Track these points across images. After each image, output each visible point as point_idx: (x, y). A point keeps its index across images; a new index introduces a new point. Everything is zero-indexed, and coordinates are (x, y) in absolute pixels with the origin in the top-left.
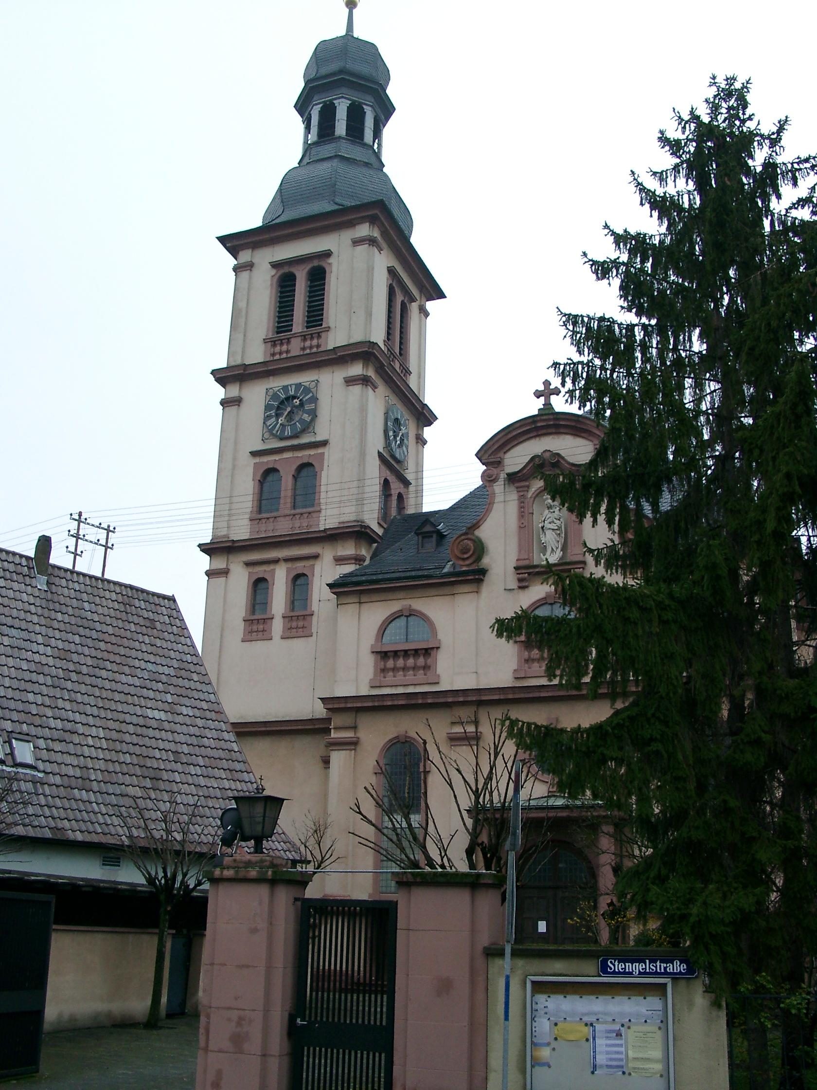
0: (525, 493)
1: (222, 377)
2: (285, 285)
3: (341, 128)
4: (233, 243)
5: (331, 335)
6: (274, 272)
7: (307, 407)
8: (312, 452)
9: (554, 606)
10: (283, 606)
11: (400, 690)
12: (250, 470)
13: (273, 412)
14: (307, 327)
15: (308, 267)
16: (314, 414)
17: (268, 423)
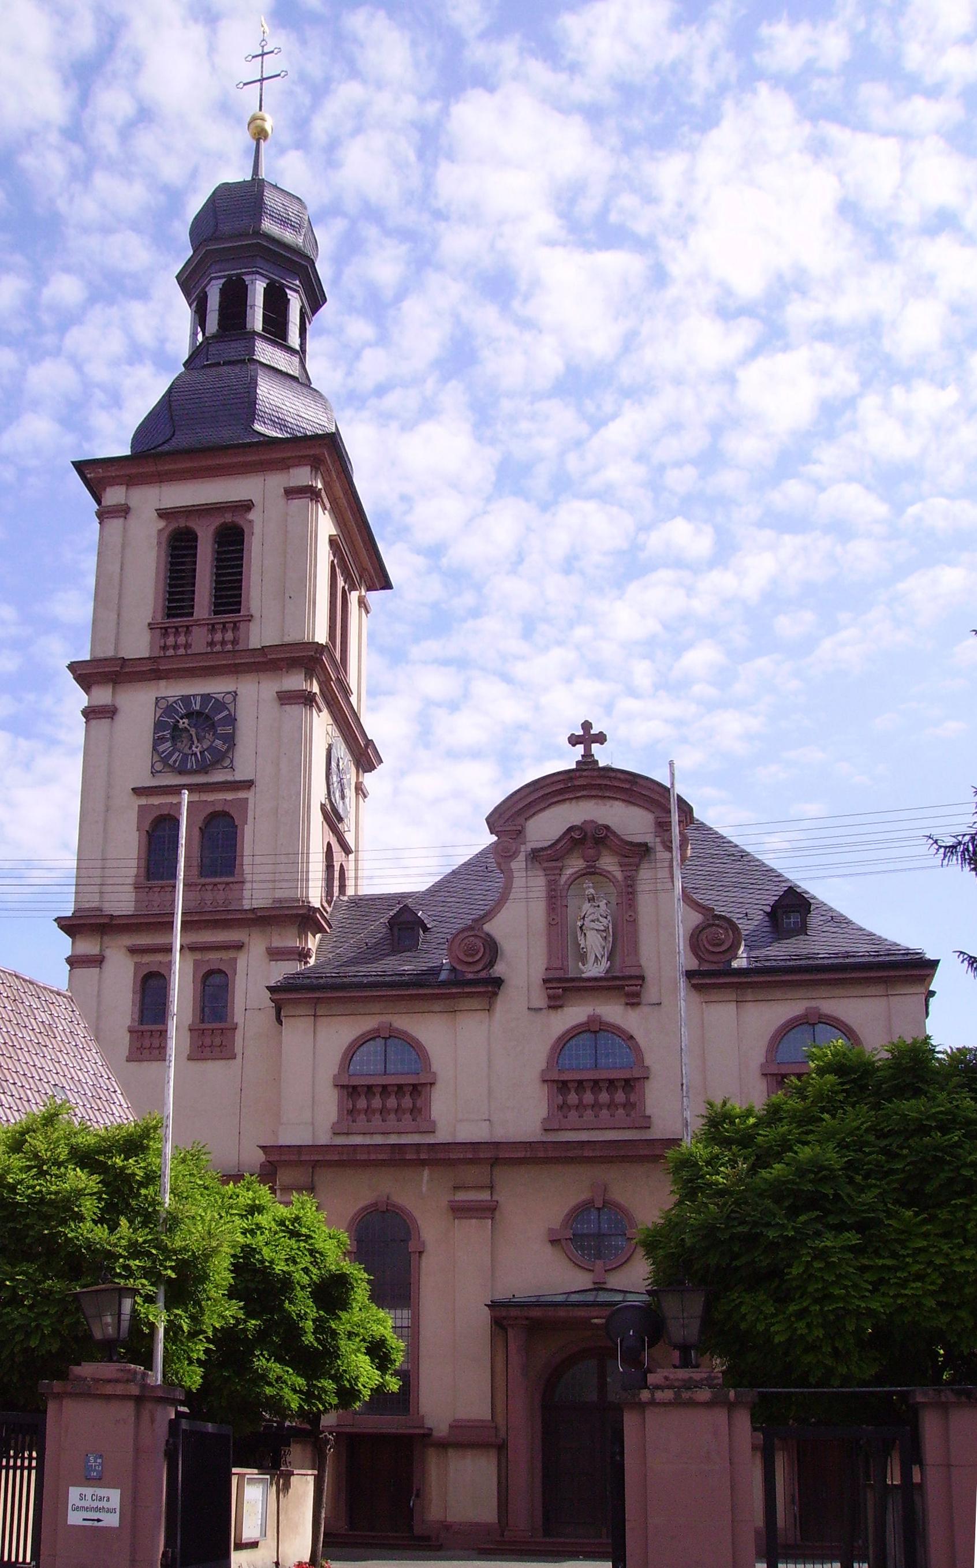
0: (557, 877)
1: (85, 674)
2: (179, 547)
3: (257, 321)
4: (95, 474)
5: (254, 628)
6: (162, 524)
7: (220, 730)
8: (229, 796)
9: (389, 1041)
10: (190, 1014)
11: (378, 1140)
12: (133, 816)
13: (167, 733)
14: (216, 613)
15: (216, 522)
16: (230, 740)
17: (161, 748)
